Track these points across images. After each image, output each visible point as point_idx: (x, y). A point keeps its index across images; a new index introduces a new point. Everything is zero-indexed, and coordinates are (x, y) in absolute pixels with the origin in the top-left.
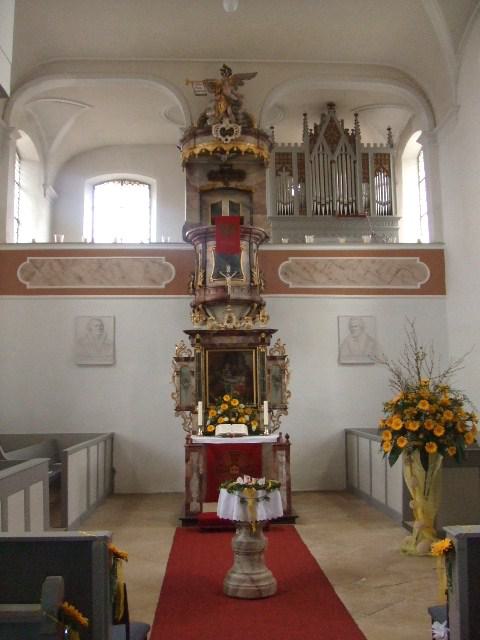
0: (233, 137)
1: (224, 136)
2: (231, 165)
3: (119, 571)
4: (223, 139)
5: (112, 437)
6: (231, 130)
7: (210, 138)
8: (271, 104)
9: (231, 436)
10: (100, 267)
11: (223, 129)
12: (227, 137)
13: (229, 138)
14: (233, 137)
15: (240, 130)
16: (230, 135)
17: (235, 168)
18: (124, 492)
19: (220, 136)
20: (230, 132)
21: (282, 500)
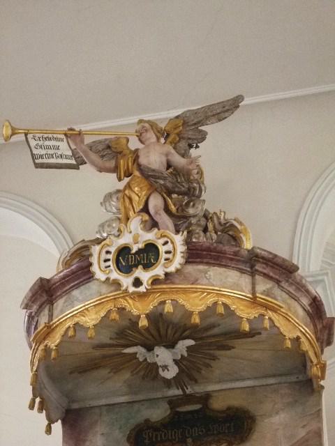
0: (159, 271)
1: (126, 269)
2: (206, 397)
3: (153, 168)
4: (126, 281)
5: (316, 297)
6: (151, 249)
7: (93, 286)
8: (309, 308)
9: (64, 237)
10: (80, 134)
11: (124, 251)
12: (139, 273)
13: (145, 276)
14: (159, 271)
15: (181, 248)
16: (147, 266)
17: (218, 404)
18: (163, 203)
19: (115, 275)
20: (149, 255)
21: (111, 127)
